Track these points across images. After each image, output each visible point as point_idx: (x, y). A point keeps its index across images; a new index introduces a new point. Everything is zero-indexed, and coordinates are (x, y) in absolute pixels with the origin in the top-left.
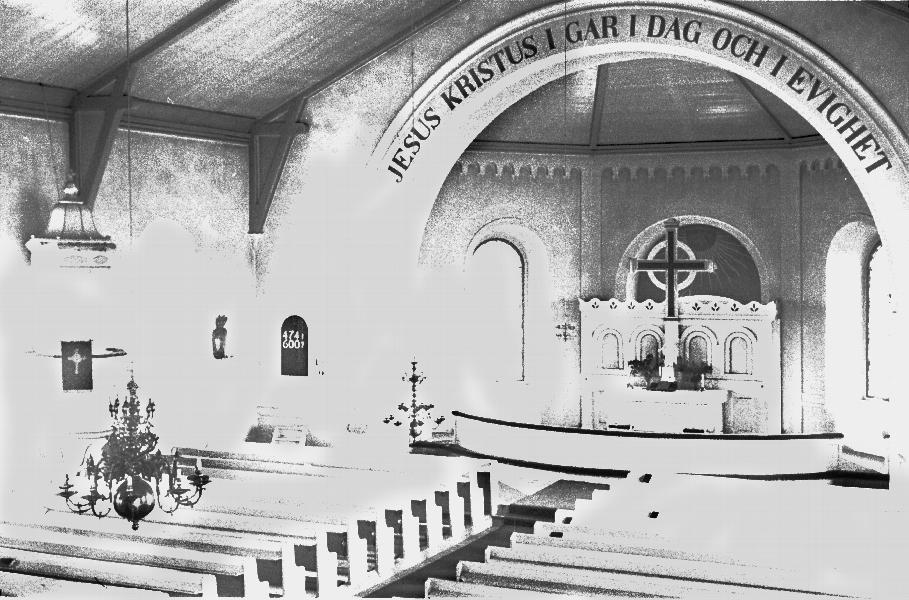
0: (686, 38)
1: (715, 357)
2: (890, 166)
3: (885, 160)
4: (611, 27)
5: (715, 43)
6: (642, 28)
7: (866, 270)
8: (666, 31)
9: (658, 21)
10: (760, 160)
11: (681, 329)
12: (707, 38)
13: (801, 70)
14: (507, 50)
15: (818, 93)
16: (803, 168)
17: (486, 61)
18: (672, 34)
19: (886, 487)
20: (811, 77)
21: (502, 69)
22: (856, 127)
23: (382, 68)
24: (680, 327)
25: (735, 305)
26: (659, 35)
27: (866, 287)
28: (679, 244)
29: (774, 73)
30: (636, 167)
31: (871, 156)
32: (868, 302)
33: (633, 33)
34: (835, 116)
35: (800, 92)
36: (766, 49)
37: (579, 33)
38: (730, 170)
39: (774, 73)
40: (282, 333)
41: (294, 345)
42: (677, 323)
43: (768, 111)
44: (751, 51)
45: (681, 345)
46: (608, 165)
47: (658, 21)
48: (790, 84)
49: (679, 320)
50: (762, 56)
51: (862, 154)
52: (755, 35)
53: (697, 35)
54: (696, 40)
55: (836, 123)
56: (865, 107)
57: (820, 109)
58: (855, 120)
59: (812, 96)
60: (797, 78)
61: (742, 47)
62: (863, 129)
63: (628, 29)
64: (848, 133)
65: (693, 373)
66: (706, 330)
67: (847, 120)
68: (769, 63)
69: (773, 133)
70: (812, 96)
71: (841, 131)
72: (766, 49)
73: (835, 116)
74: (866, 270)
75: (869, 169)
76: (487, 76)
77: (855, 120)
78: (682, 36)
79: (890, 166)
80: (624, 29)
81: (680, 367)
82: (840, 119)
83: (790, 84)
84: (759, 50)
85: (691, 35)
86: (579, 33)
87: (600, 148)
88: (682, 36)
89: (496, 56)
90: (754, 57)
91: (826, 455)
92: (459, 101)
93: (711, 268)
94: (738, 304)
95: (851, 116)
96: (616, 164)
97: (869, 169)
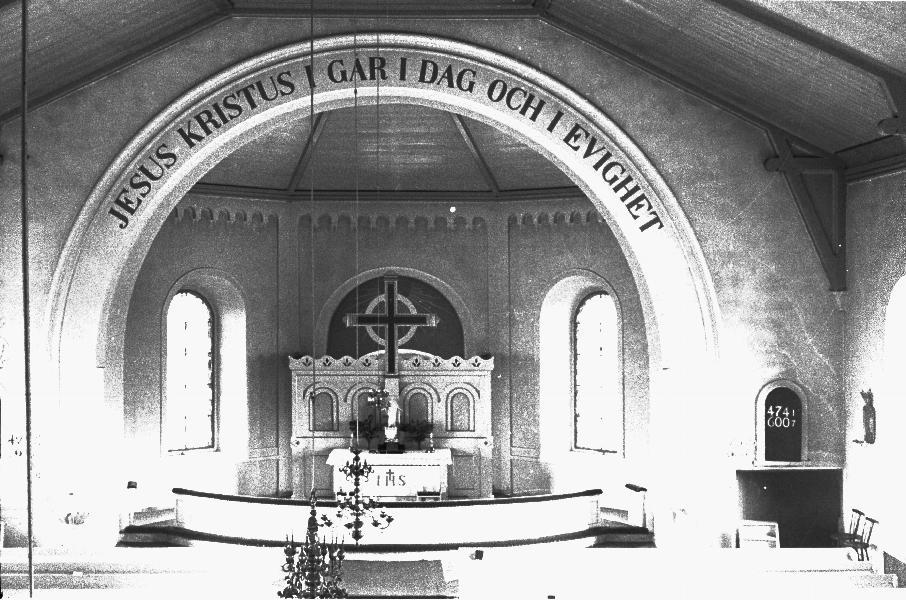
0: (460, 86)
1: (438, 413)
2: (661, 226)
3: (657, 220)
4: (378, 68)
5: (490, 94)
6: (413, 73)
7: (574, 324)
8: (439, 77)
9: (430, 67)
10: (266, 209)
11: (402, 386)
12: (481, 89)
13: (577, 127)
14: (259, 85)
15: (595, 149)
16: (512, 221)
17: (233, 96)
18: (446, 82)
19: (651, 544)
20: (587, 135)
21: (253, 106)
22: (630, 186)
23: (99, 93)
24: (400, 383)
25: (436, 361)
26: (432, 81)
27: (574, 341)
28: (400, 297)
29: (551, 128)
30: (376, 216)
31: (645, 216)
32: (576, 355)
33: (403, 78)
34: (610, 175)
35: (576, 149)
36: (542, 104)
37: (344, 74)
38: (417, 221)
39: (551, 128)
40: (767, 409)
41: (782, 422)
42: (396, 381)
43: (483, 161)
44: (527, 105)
45: (402, 403)
46: (304, 212)
47: (430, 67)
48: (567, 140)
49: (398, 377)
50: (537, 111)
51: (635, 213)
52: (530, 88)
53: (472, 85)
54: (470, 89)
55: (611, 182)
56: (638, 168)
57: (596, 167)
58: (629, 179)
59: (588, 154)
60: (572, 135)
61: (519, 100)
62: (636, 188)
63: (398, 72)
64: (623, 192)
65: (417, 434)
66: (469, 387)
67: (621, 179)
68: (545, 118)
69: (481, 184)
70: (588, 154)
71: (616, 189)
72: (542, 104)
73: (610, 175)
74: (574, 324)
75: (643, 228)
76: (234, 113)
77: (629, 179)
78: (455, 84)
79: (661, 226)
80: (392, 72)
81: (402, 427)
82: (615, 178)
83: (567, 140)
84: (534, 104)
85: (465, 85)
86: (344, 74)
87: (299, 193)
88: (455, 84)
89: (246, 91)
90: (530, 112)
91: (584, 514)
92: (200, 138)
93: (433, 322)
94: (440, 359)
95: (625, 175)
96: (316, 210)
97: (643, 228)
